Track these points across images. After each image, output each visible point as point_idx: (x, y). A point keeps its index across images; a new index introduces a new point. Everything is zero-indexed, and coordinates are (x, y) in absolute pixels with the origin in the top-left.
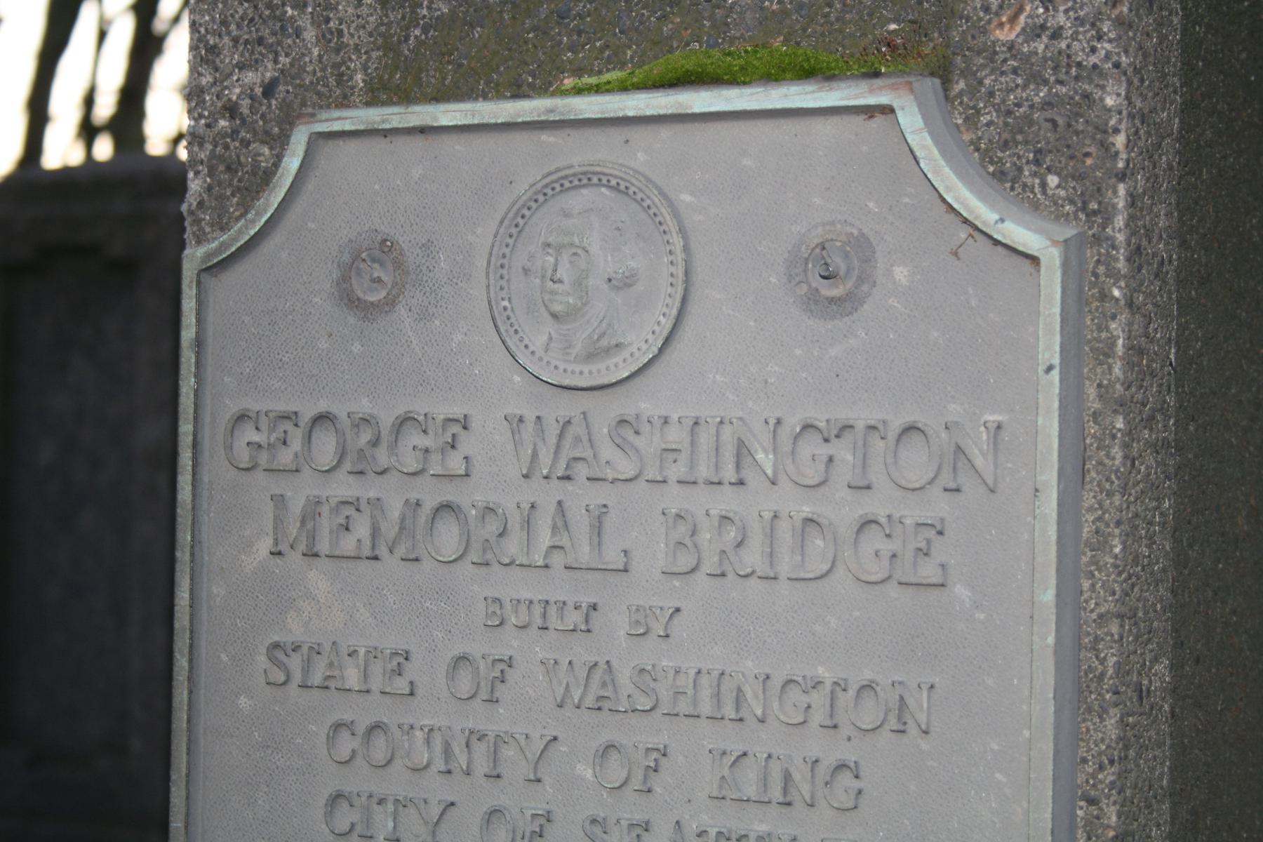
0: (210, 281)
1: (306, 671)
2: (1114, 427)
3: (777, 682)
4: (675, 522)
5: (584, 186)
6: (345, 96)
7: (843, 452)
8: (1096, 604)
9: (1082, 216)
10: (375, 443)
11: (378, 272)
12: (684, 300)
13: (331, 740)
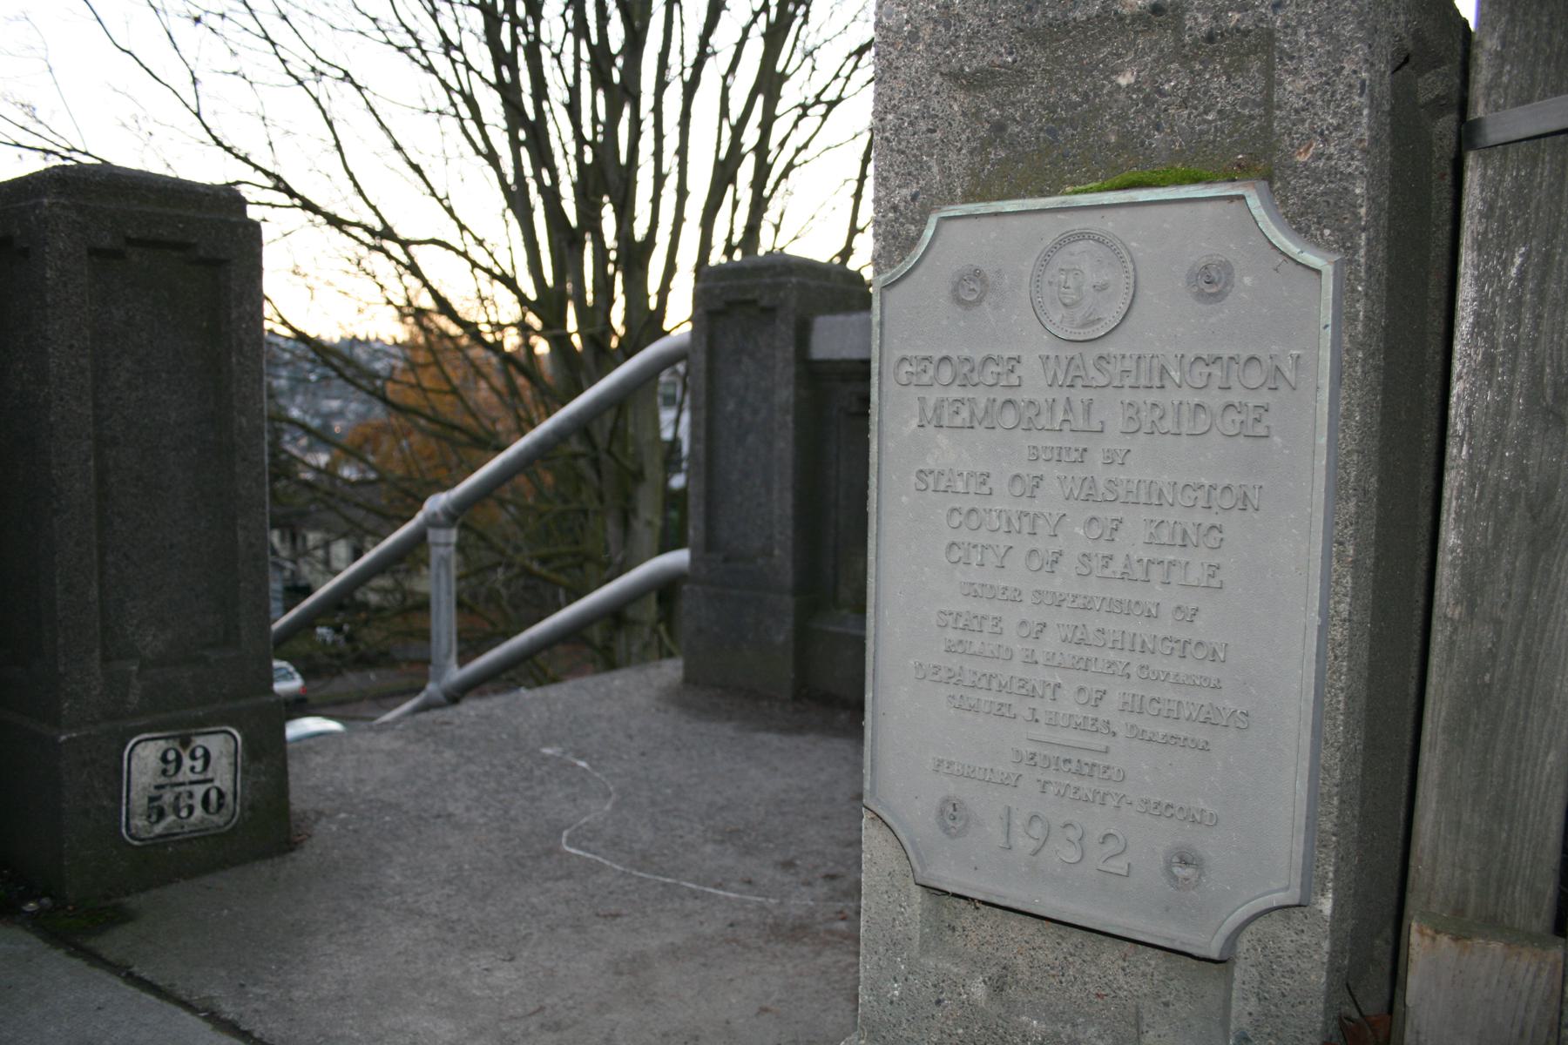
0: (886, 293)
3: (1180, 486)
4: (1152, 408)
6: (952, 200)
7: (1216, 371)
10: (972, 370)
12: (1134, 296)
13: (949, 517)
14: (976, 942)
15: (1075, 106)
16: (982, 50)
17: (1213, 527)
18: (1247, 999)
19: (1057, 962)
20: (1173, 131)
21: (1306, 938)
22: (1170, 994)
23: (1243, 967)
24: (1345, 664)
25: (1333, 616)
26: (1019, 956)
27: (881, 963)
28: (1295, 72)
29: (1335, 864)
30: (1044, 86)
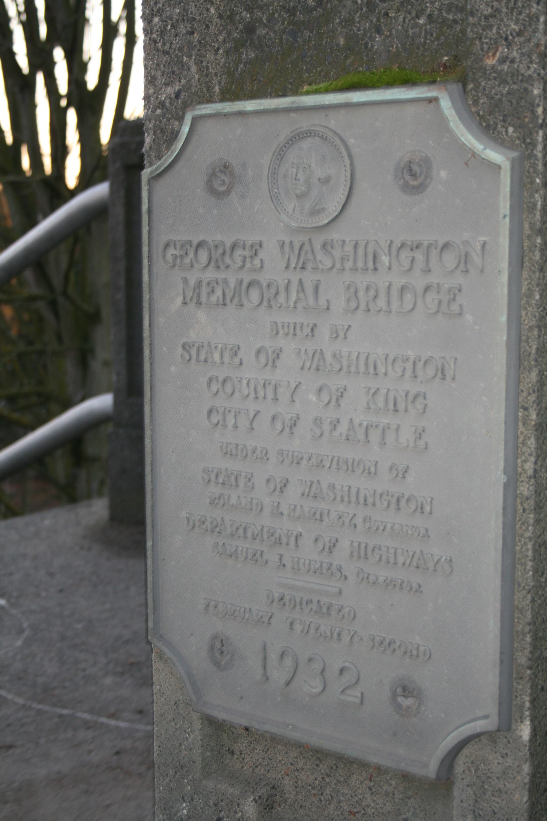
1: (198, 354)
2: (536, 242)
5: (309, 136)
6: (211, 96)
8: (528, 322)
9: (523, 146)
10: (224, 254)
11: (223, 177)
14: (251, 764)
19: (317, 782)
20: (391, 34)
21: (509, 761)
25: (521, 474)
26: (286, 777)
29: (531, 694)
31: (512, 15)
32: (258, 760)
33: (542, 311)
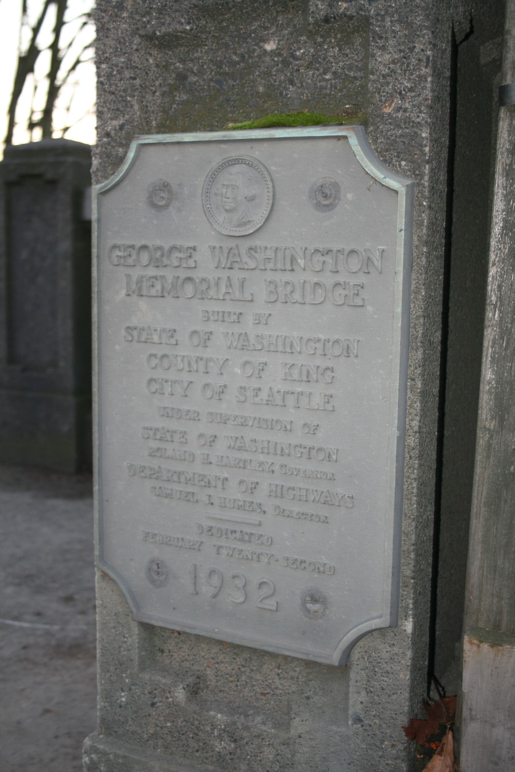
5: (237, 164)
7: (328, 259)
9: (413, 176)
10: (162, 256)
14: (178, 660)
15: (234, 64)
16: (168, 20)
17: (327, 369)
18: (359, 693)
19: (234, 672)
20: (302, 86)
21: (396, 649)
22: (310, 691)
23: (356, 670)
24: (417, 462)
25: (408, 430)
26: (208, 669)
27: (112, 679)
28: (383, 48)
29: (413, 598)
30: (214, 48)
31: (405, 75)
32: (184, 656)
33: (426, 304)
